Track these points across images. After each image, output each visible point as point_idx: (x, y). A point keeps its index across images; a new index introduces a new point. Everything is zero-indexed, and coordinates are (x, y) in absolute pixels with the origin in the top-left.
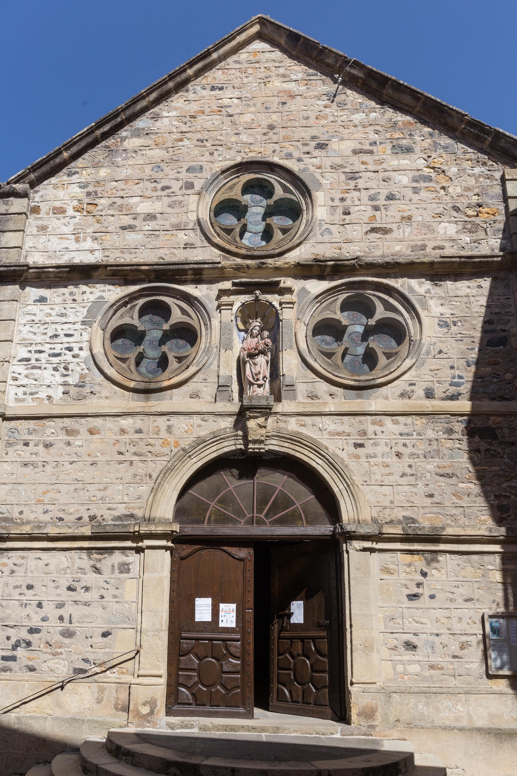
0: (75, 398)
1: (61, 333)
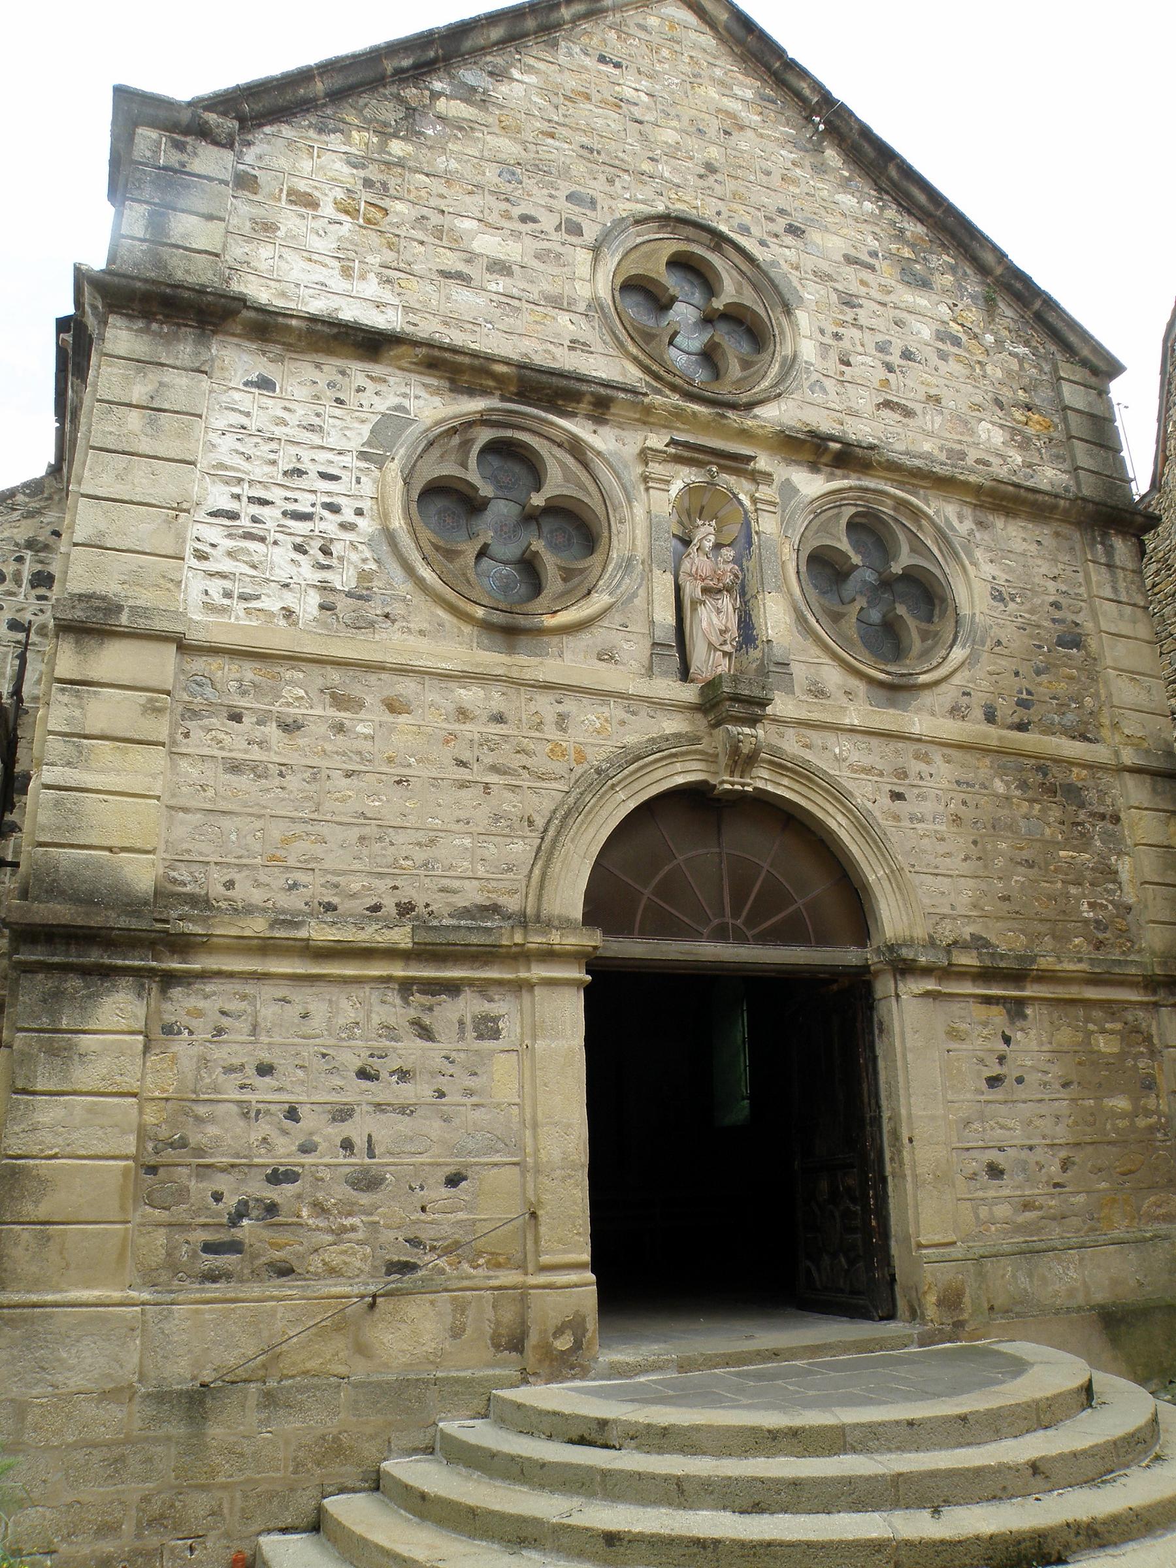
0: (349, 622)
1: (313, 469)
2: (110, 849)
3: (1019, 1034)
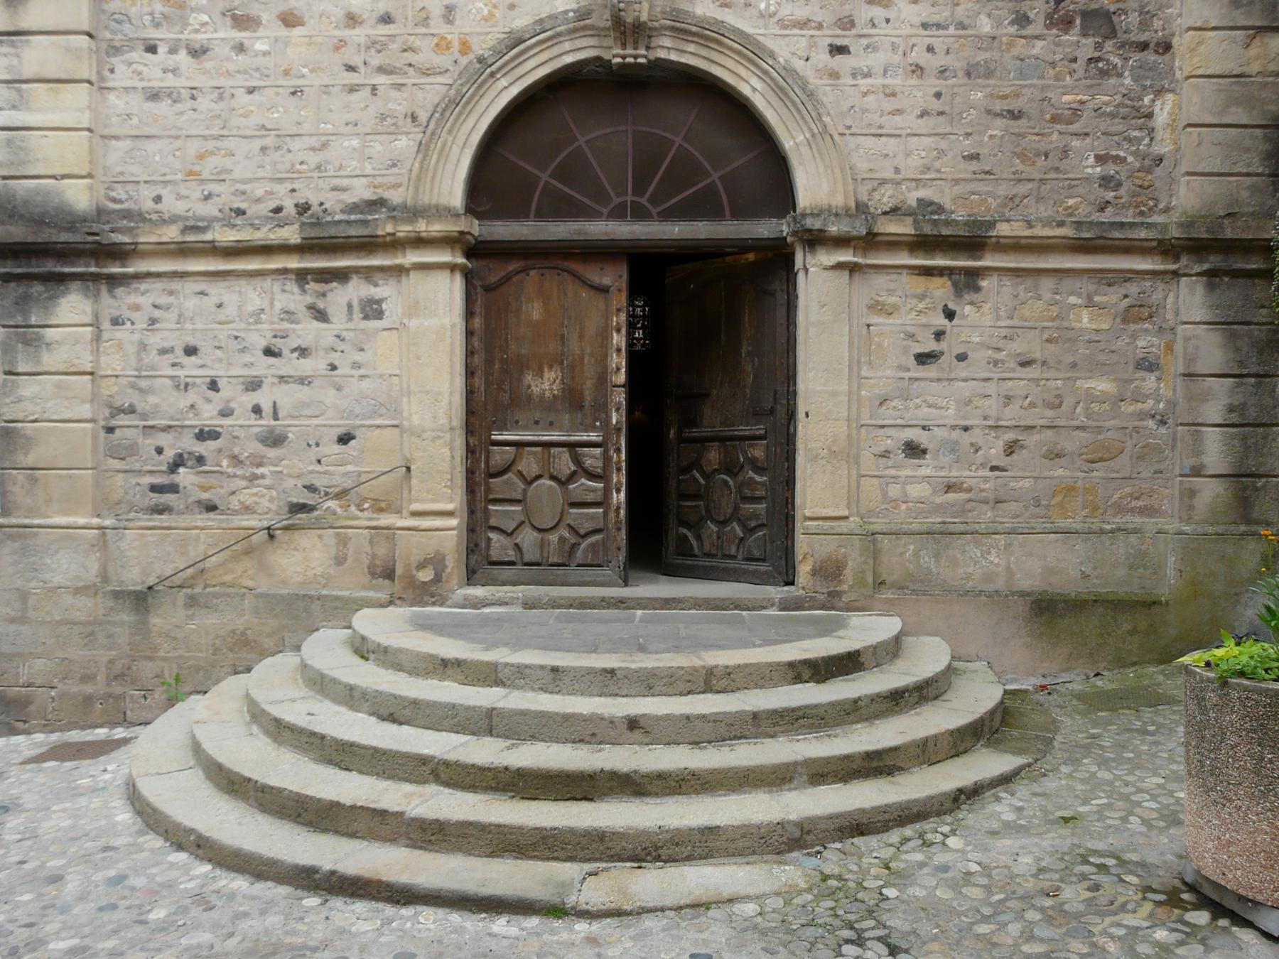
2: (54, 177)
3: (968, 309)
